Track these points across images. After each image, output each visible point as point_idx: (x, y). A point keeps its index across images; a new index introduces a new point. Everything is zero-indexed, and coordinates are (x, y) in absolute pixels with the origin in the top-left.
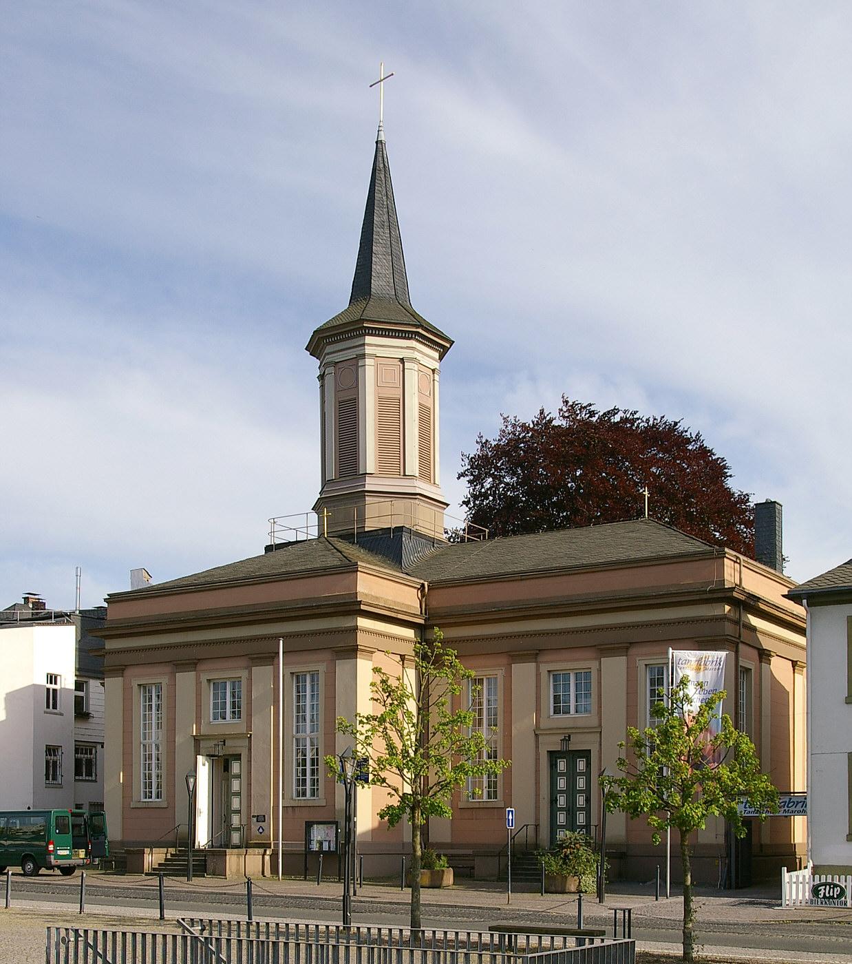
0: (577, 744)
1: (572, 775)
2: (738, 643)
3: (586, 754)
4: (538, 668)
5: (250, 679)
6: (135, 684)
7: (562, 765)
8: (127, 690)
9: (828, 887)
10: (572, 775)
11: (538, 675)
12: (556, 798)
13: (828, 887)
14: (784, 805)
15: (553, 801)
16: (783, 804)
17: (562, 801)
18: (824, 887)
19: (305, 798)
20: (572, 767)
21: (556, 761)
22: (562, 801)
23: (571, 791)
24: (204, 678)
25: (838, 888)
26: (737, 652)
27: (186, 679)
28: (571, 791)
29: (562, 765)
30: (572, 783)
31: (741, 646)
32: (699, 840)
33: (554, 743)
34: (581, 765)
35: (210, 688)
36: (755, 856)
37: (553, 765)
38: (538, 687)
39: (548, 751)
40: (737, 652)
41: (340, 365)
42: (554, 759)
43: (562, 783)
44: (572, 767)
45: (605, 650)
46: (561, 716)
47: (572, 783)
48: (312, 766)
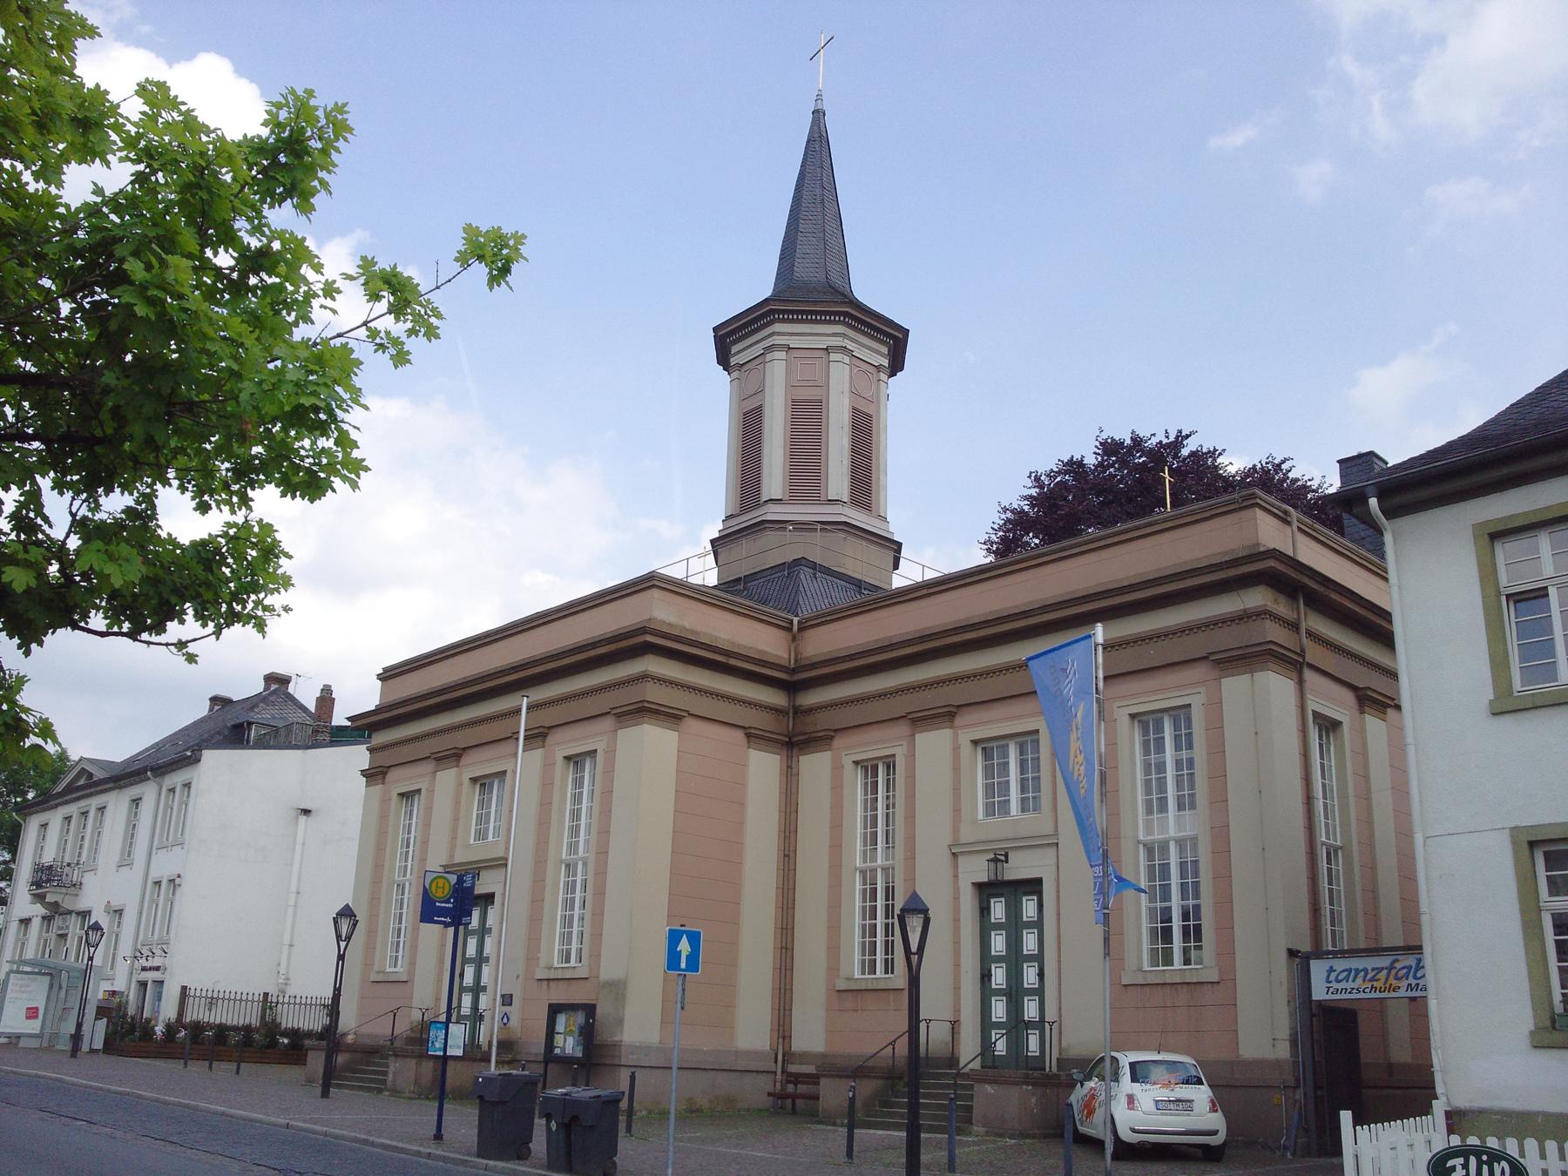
0: (1019, 868)
1: (1014, 927)
2: (1301, 664)
3: (1033, 886)
4: (956, 738)
5: (911, 756)
6: (847, 761)
7: (998, 910)
8: (837, 768)
9: (1473, 1160)
10: (1014, 927)
11: (956, 748)
12: (990, 971)
13: (1473, 1160)
14: (1409, 973)
15: (986, 976)
16: (1405, 971)
17: (999, 977)
18: (1461, 1160)
19: (873, 976)
20: (1014, 911)
21: (989, 903)
22: (999, 977)
23: (1015, 959)
24: (965, 737)
25: (1504, 1163)
26: (1301, 682)
27: (934, 744)
28: (1015, 959)
29: (998, 910)
30: (1014, 943)
31: (1309, 675)
32: (1241, 1052)
33: (977, 869)
34: (1029, 908)
35: (857, 773)
36: (1369, 1087)
37: (984, 910)
38: (956, 769)
39: (973, 883)
40: (1301, 682)
41: (746, 367)
42: (986, 898)
43: (998, 943)
44: (1014, 911)
45: (921, 720)
46: (997, 819)
47: (1014, 943)
48: (886, 919)
